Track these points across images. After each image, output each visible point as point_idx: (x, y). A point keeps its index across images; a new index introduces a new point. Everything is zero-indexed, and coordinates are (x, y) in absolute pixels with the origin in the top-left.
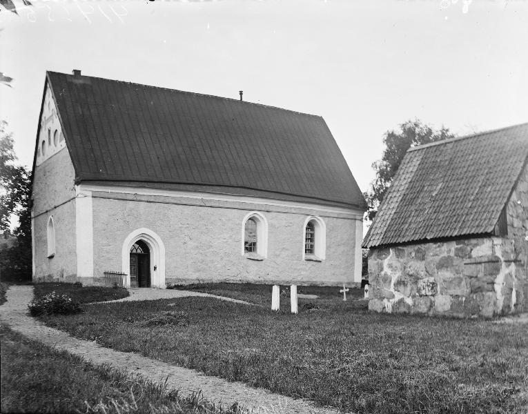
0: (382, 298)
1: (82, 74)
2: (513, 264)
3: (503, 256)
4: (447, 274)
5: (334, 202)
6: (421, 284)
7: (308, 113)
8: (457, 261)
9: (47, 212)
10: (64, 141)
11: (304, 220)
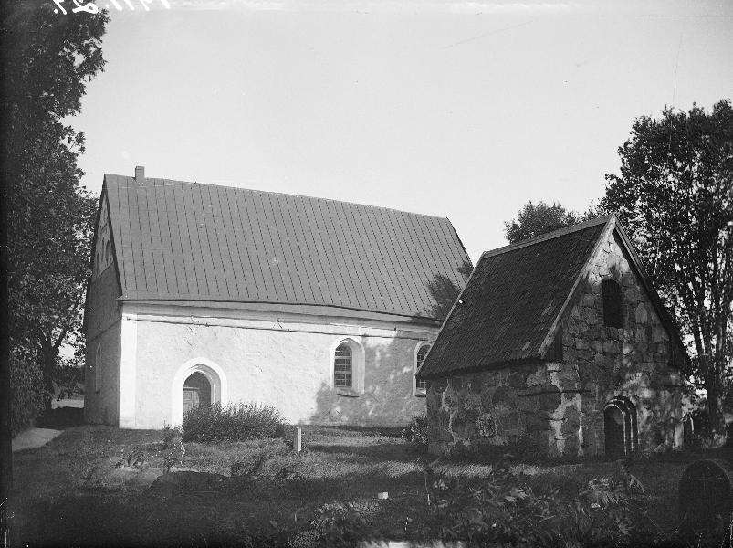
0: (440, 442)
1: (146, 176)
2: (578, 395)
3: (561, 385)
4: (503, 409)
5: (214, 309)
6: (478, 423)
7: (190, 179)
8: (513, 394)
9: (97, 337)
10: (663, 333)
11: (414, 345)
